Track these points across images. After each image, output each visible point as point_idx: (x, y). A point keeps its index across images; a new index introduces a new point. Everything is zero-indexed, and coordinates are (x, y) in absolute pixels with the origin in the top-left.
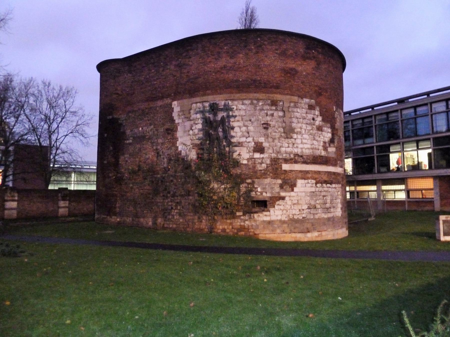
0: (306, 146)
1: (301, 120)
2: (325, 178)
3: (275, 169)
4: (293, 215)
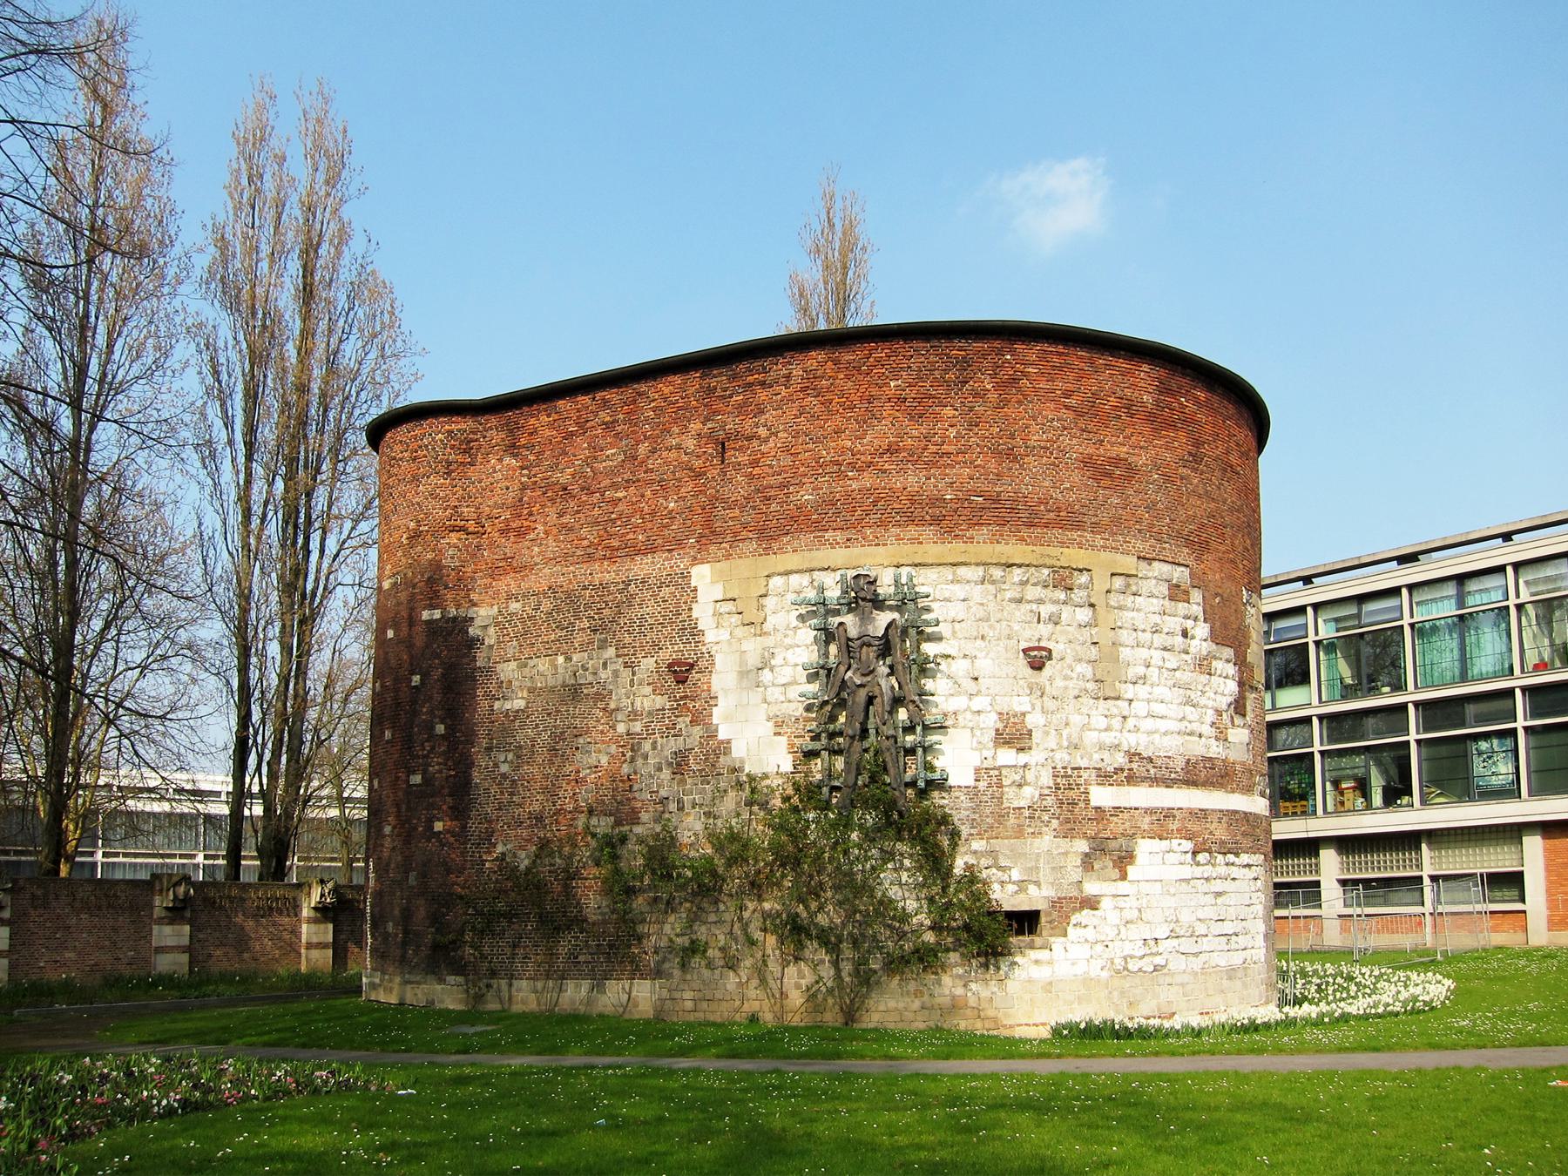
0: (1163, 725)
1: (1148, 635)
2: (1220, 832)
3: (1067, 804)
4: (1125, 958)
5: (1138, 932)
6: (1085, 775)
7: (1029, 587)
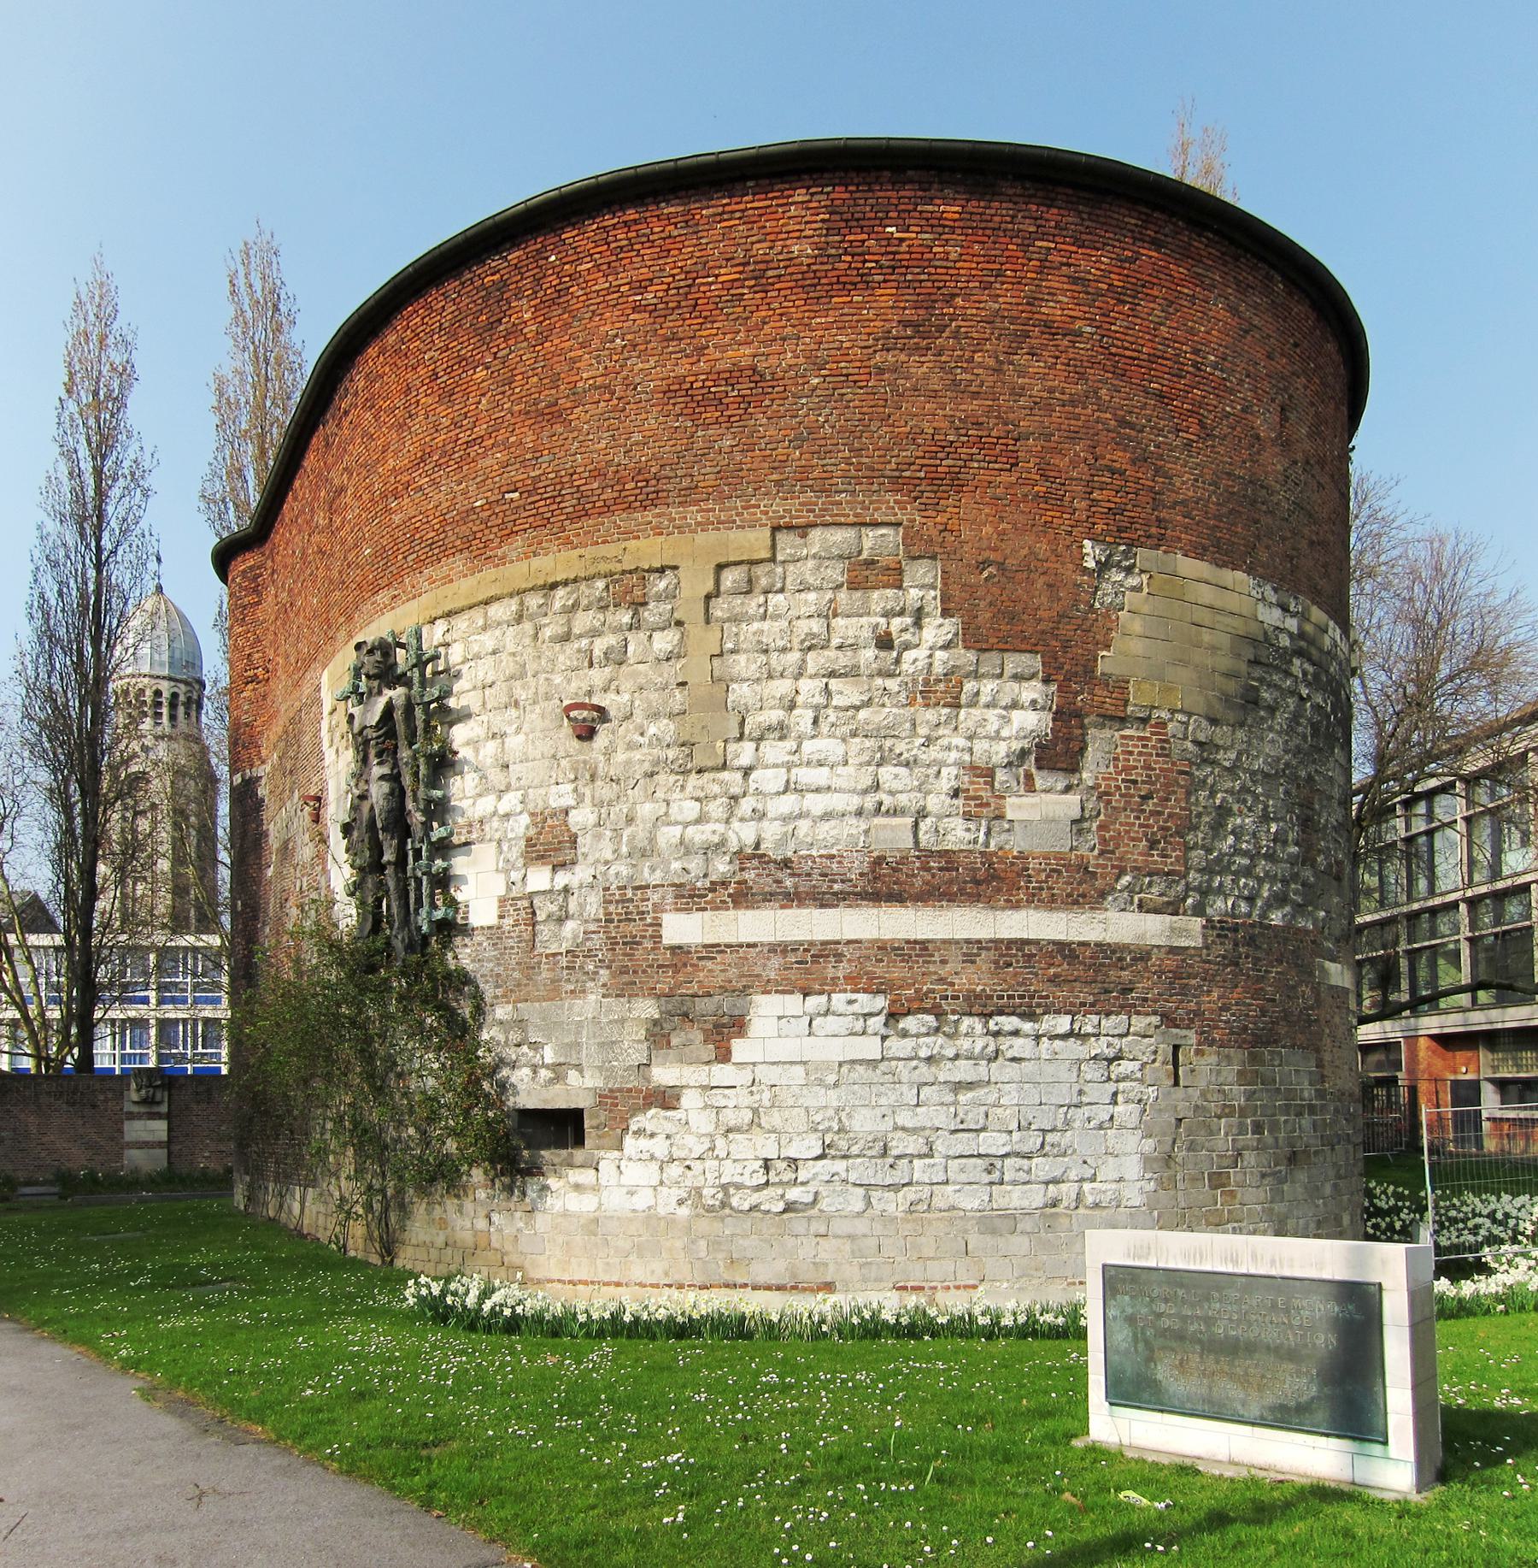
0: (816, 804)
3: (627, 948)
4: (724, 1188)
5: (751, 1148)
6: (655, 897)
7: (580, 614)
